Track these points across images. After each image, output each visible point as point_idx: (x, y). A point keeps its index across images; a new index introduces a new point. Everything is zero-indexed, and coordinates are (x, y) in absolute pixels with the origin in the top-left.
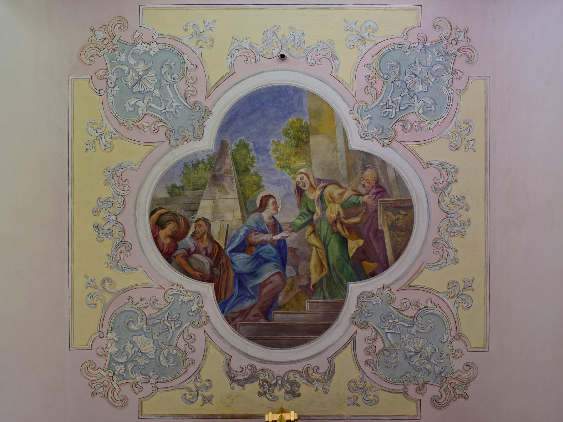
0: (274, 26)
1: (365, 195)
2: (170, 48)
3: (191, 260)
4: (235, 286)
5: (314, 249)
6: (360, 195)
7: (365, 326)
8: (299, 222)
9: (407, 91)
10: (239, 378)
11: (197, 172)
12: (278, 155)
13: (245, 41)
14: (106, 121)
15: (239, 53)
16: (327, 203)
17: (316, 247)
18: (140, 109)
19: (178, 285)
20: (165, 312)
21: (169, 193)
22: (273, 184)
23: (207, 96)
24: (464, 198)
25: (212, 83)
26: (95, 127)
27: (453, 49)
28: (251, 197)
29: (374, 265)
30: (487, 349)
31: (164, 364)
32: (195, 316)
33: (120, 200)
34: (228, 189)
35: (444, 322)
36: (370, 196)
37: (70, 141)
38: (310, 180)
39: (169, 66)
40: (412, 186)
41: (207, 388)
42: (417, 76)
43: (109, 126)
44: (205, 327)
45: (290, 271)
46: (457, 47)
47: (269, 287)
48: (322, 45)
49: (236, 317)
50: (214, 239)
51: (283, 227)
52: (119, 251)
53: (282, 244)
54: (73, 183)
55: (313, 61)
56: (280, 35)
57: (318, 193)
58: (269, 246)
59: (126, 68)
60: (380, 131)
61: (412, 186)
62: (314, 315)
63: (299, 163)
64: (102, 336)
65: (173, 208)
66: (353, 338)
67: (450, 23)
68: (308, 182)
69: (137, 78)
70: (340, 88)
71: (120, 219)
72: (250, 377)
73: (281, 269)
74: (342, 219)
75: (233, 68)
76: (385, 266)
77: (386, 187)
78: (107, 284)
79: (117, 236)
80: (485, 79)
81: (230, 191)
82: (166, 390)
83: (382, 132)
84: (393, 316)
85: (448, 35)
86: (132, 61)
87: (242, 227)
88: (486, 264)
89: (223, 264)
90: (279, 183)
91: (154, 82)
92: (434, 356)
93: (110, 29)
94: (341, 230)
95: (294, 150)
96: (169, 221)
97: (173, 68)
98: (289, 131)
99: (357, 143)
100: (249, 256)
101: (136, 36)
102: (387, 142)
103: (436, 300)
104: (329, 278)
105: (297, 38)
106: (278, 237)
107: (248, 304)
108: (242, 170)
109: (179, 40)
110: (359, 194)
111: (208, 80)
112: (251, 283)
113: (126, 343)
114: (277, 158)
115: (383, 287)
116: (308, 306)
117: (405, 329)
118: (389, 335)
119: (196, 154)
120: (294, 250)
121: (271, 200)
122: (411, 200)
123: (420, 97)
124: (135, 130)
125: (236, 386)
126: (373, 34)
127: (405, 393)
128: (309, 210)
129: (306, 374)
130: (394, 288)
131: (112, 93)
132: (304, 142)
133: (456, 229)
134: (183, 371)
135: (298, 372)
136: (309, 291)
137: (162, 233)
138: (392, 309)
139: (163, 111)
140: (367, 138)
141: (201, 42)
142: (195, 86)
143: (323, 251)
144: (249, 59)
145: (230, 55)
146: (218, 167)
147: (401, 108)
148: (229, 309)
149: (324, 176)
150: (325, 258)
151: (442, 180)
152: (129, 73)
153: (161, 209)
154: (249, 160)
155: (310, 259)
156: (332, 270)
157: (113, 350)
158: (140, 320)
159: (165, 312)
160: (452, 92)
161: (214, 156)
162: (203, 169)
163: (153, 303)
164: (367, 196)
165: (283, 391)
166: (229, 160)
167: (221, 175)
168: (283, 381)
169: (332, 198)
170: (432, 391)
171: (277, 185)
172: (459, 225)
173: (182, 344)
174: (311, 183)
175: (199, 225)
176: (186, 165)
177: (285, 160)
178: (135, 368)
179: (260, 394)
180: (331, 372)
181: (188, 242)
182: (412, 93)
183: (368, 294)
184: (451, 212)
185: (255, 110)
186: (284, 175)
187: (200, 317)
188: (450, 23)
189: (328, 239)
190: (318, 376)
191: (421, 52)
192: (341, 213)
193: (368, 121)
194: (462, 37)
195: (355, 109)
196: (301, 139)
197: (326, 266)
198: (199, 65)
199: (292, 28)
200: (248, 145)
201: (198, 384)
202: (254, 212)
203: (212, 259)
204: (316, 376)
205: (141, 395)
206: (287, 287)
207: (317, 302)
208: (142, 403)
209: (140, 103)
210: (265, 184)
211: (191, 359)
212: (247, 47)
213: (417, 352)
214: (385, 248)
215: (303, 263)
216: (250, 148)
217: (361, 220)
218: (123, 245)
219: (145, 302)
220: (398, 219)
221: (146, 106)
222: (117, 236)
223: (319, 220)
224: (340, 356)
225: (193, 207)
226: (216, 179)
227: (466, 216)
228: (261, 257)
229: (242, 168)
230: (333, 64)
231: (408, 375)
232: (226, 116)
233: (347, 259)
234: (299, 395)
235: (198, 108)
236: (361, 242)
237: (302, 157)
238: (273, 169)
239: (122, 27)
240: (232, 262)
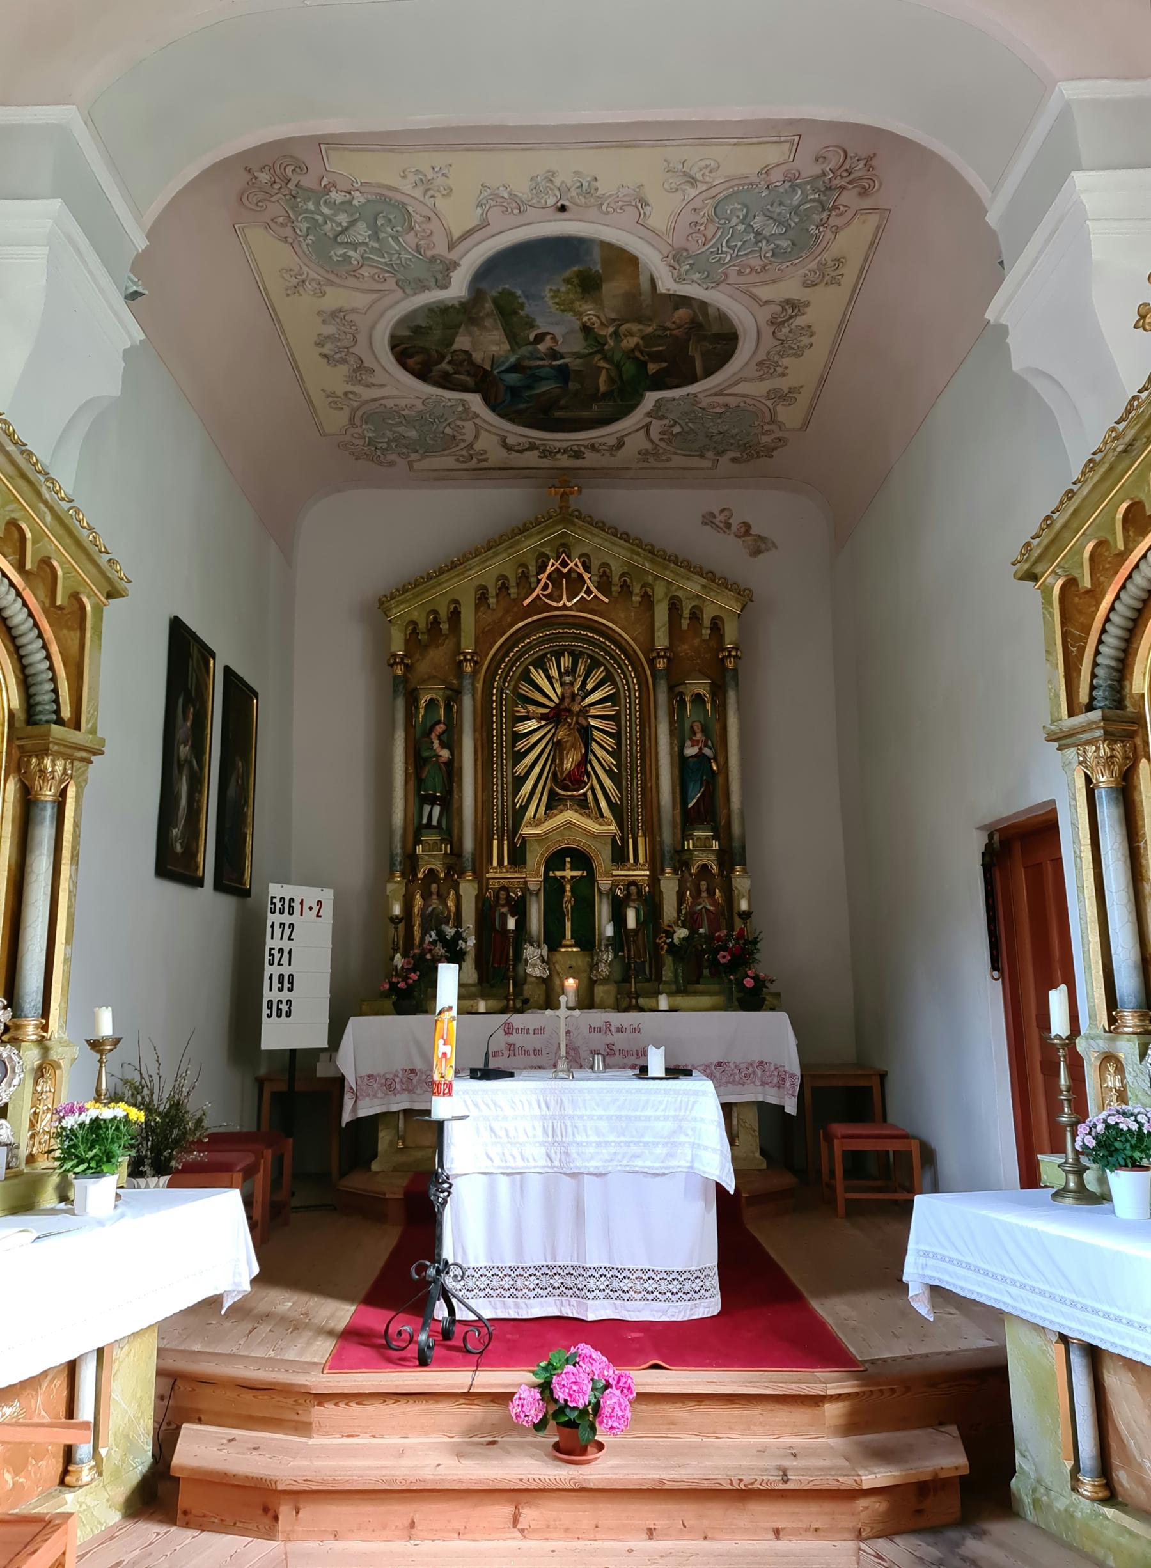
15: (493, 203)
24: (809, 327)
57: (611, 329)
58: (548, 369)
59: (320, 218)
76: (694, 380)
86: (326, 210)
103: (749, 401)
105: (585, 185)
106: (560, 362)
107: (522, 406)
129: (593, 448)
145: (480, 205)
173: (448, 431)
182: (759, 238)
196: (589, 285)
198: (433, 216)
199: (576, 173)
209: (351, 253)
212: (506, 196)
221: (362, 256)
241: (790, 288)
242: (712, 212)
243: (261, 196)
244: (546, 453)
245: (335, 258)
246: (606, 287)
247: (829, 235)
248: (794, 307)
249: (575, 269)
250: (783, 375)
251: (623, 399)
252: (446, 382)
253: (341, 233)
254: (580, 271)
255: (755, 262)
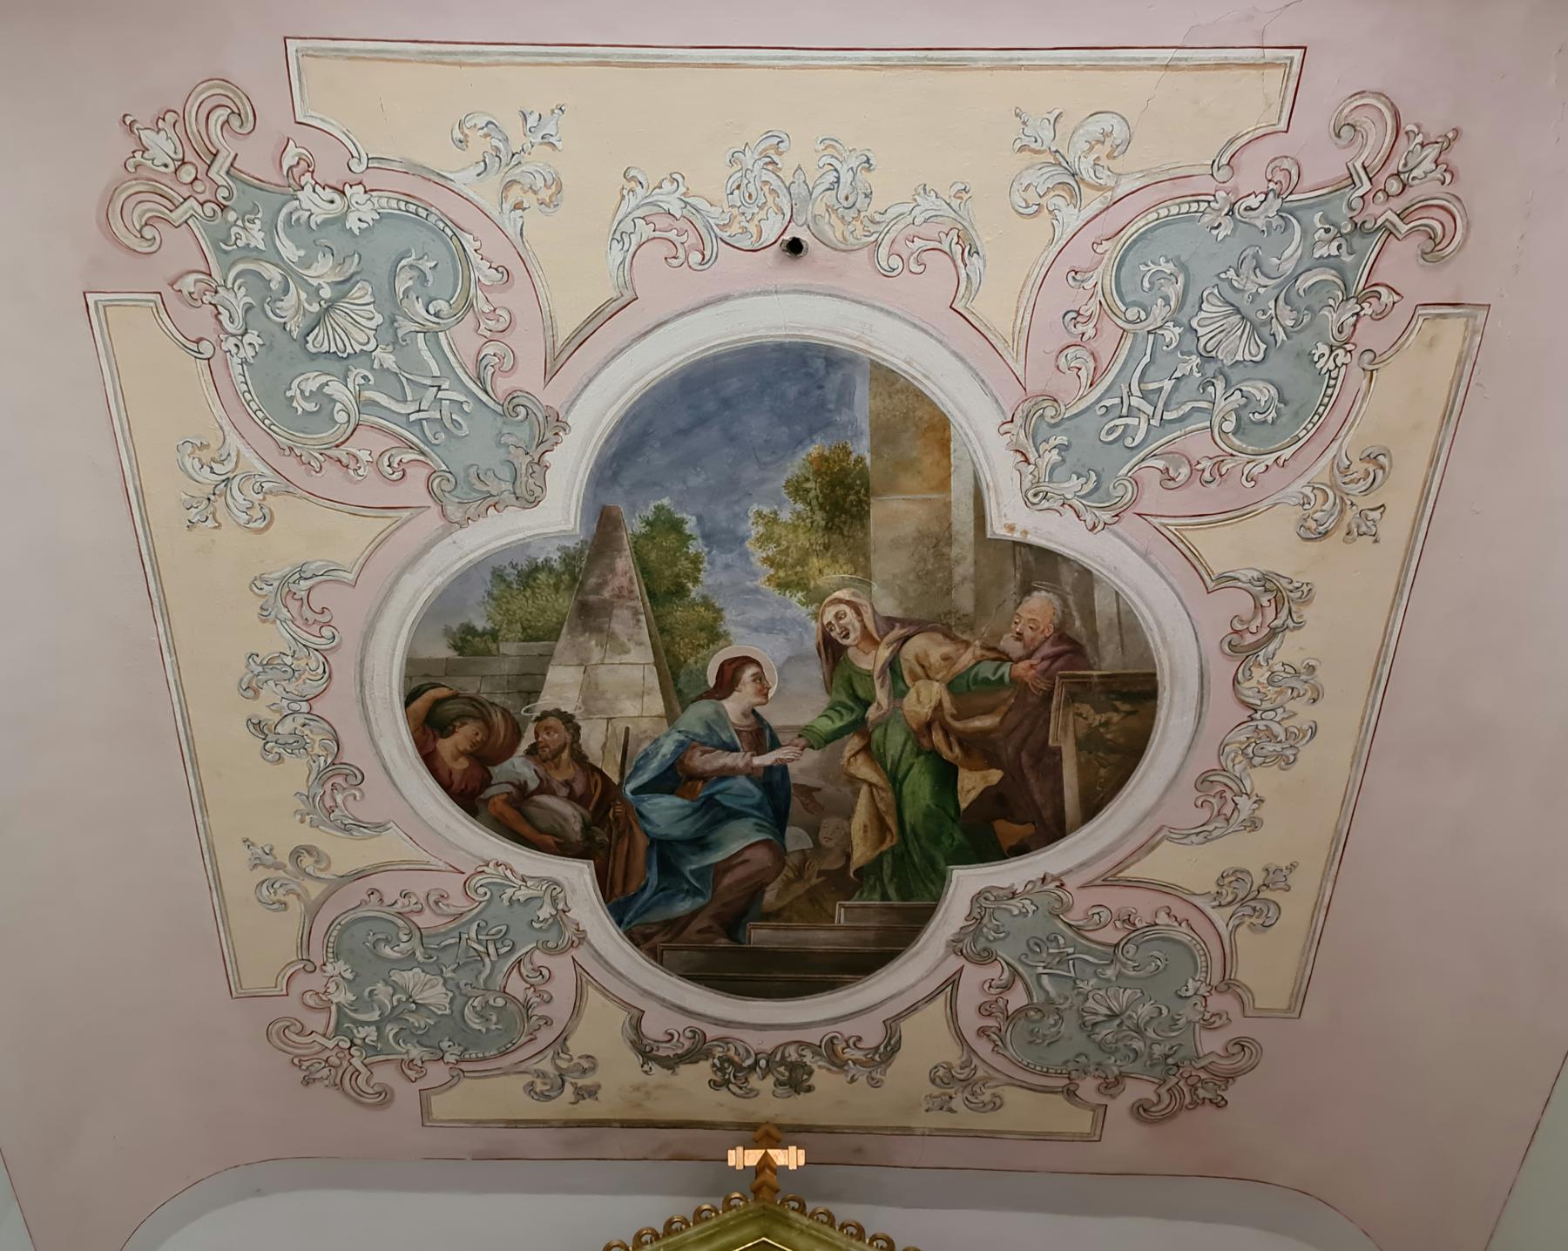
0: (769, 135)
1: (1020, 659)
2: (412, 208)
3: (532, 810)
4: (650, 868)
5: (865, 789)
6: (1004, 661)
7: (985, 958)
8: (827, 726)
9: (1196, 360)
10: (662, 1053)
11: (534, 593)
12: (771, 550)
13: (667, 186)
14: (234, 441)
15: (646, 231)
16: (908, 681)
17: (871, 785)
18: (338, 406)
19: (497, 865)
20: (471, 921)
21: (455, 647)
22: (756, 630)
23: (550, 373)
25: (565, 330)
26: (206, 455)
27: (1380, 211)
28: (691, 661)
29: (1026, 830)
30: (1296, 1014)
31: (477, 1027)
32: (547, 931)
33: (315, 661)
34: (624, 639)
35: (1194, 957)
36: (1033, 661)
37: (134, 499)
38: (862, 621)
39: (415, 273)
40: (1164, 639)
41: (584, 1071)
42: (1238, 311)
43: (247, 454)
44: (574, 952)
45: (796, 840)
46: (1398, 204)
47: (740, 872)
48: (928, 203)
49: (654, 934)
50: (591, 760)
51: (781, 737)
52: (328, 786)
53: (777, 776)
54: (166, 614)
55: (896, 262)
56: (787, 164)
57: (884, 653)
58: (742, 782)
59: (273, 273)
60: (1091, 485)
61: (1164, 639)
62: (855, 934)
63: (832, 575)
64: (310, 967)
65: (470, 686)
66: (953, 982)
67: (1396, 115)
68: (857, 625)
69: (315, 308)
70: (978, 346)
71: (318, 708)
72: (689, 1052)
73: (774, 834)
74: (949, 719)
75: (629, 284)
76: (1054, 830)
77: (1084, 642)
78: (307, 861)
79: (317, 750)
80: (1467, 316)
81: (631, 645)
82: (485, 1074)
83: (1096, 489)
84: (1062, 941)
85: (1378, 162)
86: (289, 251)
87: (667, 735)
88: (1337, 831)
89: (616, 819)
90: (770, 627)
91: (372, 324)
92: (1155, 1023)
93: (193, 128)
94: (944, 748)
95: (819, 538)
96: (462, 717)
97: (430, 277)
98: (808, 485)
99: (1012, 517)
100: (687, 802)
101: (288, 161)
102: (1106, 516)
103: (1180, 910)
104: (901, 857)
105: (846, 177)
106: (768, 759)
107: (683, 907)
108: (664, 591)
109: (440, 180)
110: (1003, 657)
111: (550, 326)
112: (691, 863)
113: (375, 983)
114: (770, 561)
115: (1044, 879)
116: (840, 916)
117: (1090, 970)
118: (1045, 980)
119: (524, 545)
120: (807, 791)
121: (750, 672)
122: (1154, 675)
123: (1234, 379)
124: (331, 469)
125: (656, 1068)
126: (1110, 163)
127: (1070, 1093)
128: (856, 698)
129: (831, 1053)
130: (1071, 883)
131: (242, 354)
132: (853, 517)
133: (1270, 747)
134: (524, 1039)
135: (809, 1045)
136: (844, 882)
137: (446, 747)
138: (1061, 926)
139: (412, 418)
140: (1045, 504)
141: (516, 189)
142: (509, 339)
143: (889, 796)
144: (681, 254)
145: (619, 237)
146: (592, 581)
147: (1167, 416)
148: (636, 916)
149: (906, 610)
150: (893, 810)
151: (1258, 621)
152: (286, 291)
153: (435, 686)
154: (684, 564)
155: (853, 811)
156: (910, 837)
157: (344, 996)
158: (405, 938)
159: (471, 921)
160: (1347, 359)
161: (582, 552)
162: (548, 586)
163: (437, 903)
164: (1024, 664)
165: (770, 1080)
166: (625, 563)
167: (605, 601)
168: (770, 1062)
169: (923, 667)
170: (1135, 1091)
171: (769, 633)
172: (1282, 737)
173: (516, 987)
174: (864, 627)
175: (548, 729)
176: (498, 575)
177: (793, 567)
178: (403, 1033)
179: (715, 1085)
180: (890, 1048)
181: (519, 767)
182: (1211, 369)
183: (1001, 893)
184: (1266, 705)
185: (702, 421)
186: (789, 606)
187: (561, 933)
188: (1396, 115)
189: (904, 767)
190: (858, 1055)
191: (1269, 225)
192: (947, 704)
193: (1054, 456)
194: (1428, 165)
195: (1018, 420)
196: (842, 501)
197: (894, 829)
199: (830, 143)
200: (683, 521)
201: (563, 1065)
202: (701, 698)
203: (586, 808)
204: (851, 1054)
205: (422, 1084)
206: (788, 873)
207: (864, 907)
208: (428, 1099)
209: (335, 389)
210: (733, 629)
211: (541, 1018)
213: (1113, 1016)
214: (1059, 791)
215: (829, 825)
216: (688, 532)
217: (1002, 722)
218: (338, 772)
219: (413, 900)
220: (1106, 724)
221: (358, 398)
222: (317, 750)
223: (884, 722)
224: (916, 1017)
225: (526, 684)
226: (590, 615)
227: (1305, 713)
228: (719, 804)
229: (665, 585)
230: (963, 272)
231: (1082, 1059)
232: (611, 435)
233: (952, 812)
234: (810, 1089)
235: (522, 410)
236: (995, 776)
237: (842, 560)
238: (756, 591)
239: (235, 122)
240: (641, 815)
241: (1264, 543)
242: (1109, 283)
243: (153, 206)
244: (732, 1072)
245: (301, 405)
246: (879, 510)
247: (1357, 380)
248: (1279, 596)
249: (813, 450)
250: (1254, 824)
251: (902, 892)
252: (518, 822)
253: (318, 321)
254: (823, 458)
255: (1201, 447)
